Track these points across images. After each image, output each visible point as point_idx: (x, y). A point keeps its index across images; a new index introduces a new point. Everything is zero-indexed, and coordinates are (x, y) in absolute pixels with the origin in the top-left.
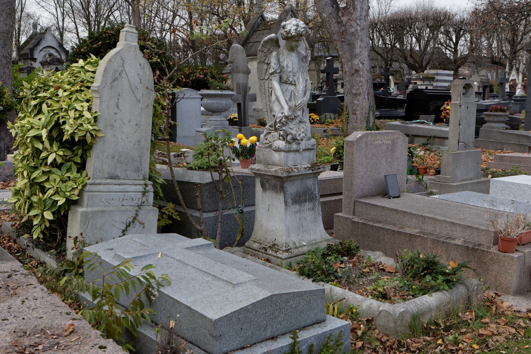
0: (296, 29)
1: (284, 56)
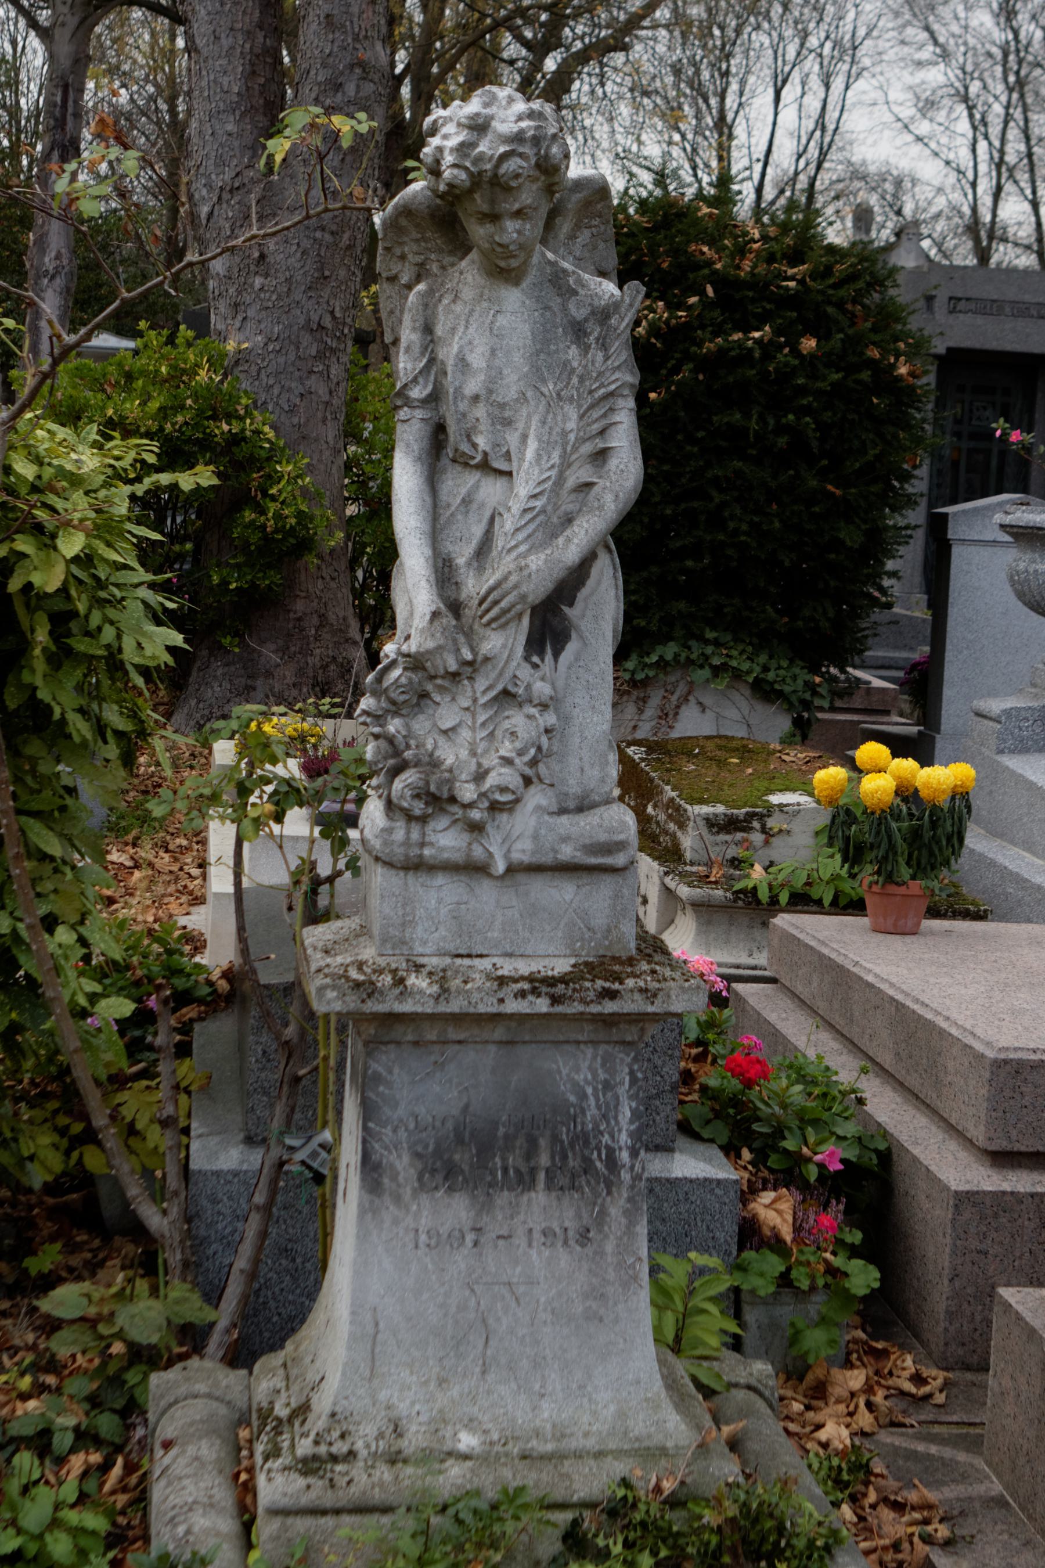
0: (463, 149)
1: (458, 308)
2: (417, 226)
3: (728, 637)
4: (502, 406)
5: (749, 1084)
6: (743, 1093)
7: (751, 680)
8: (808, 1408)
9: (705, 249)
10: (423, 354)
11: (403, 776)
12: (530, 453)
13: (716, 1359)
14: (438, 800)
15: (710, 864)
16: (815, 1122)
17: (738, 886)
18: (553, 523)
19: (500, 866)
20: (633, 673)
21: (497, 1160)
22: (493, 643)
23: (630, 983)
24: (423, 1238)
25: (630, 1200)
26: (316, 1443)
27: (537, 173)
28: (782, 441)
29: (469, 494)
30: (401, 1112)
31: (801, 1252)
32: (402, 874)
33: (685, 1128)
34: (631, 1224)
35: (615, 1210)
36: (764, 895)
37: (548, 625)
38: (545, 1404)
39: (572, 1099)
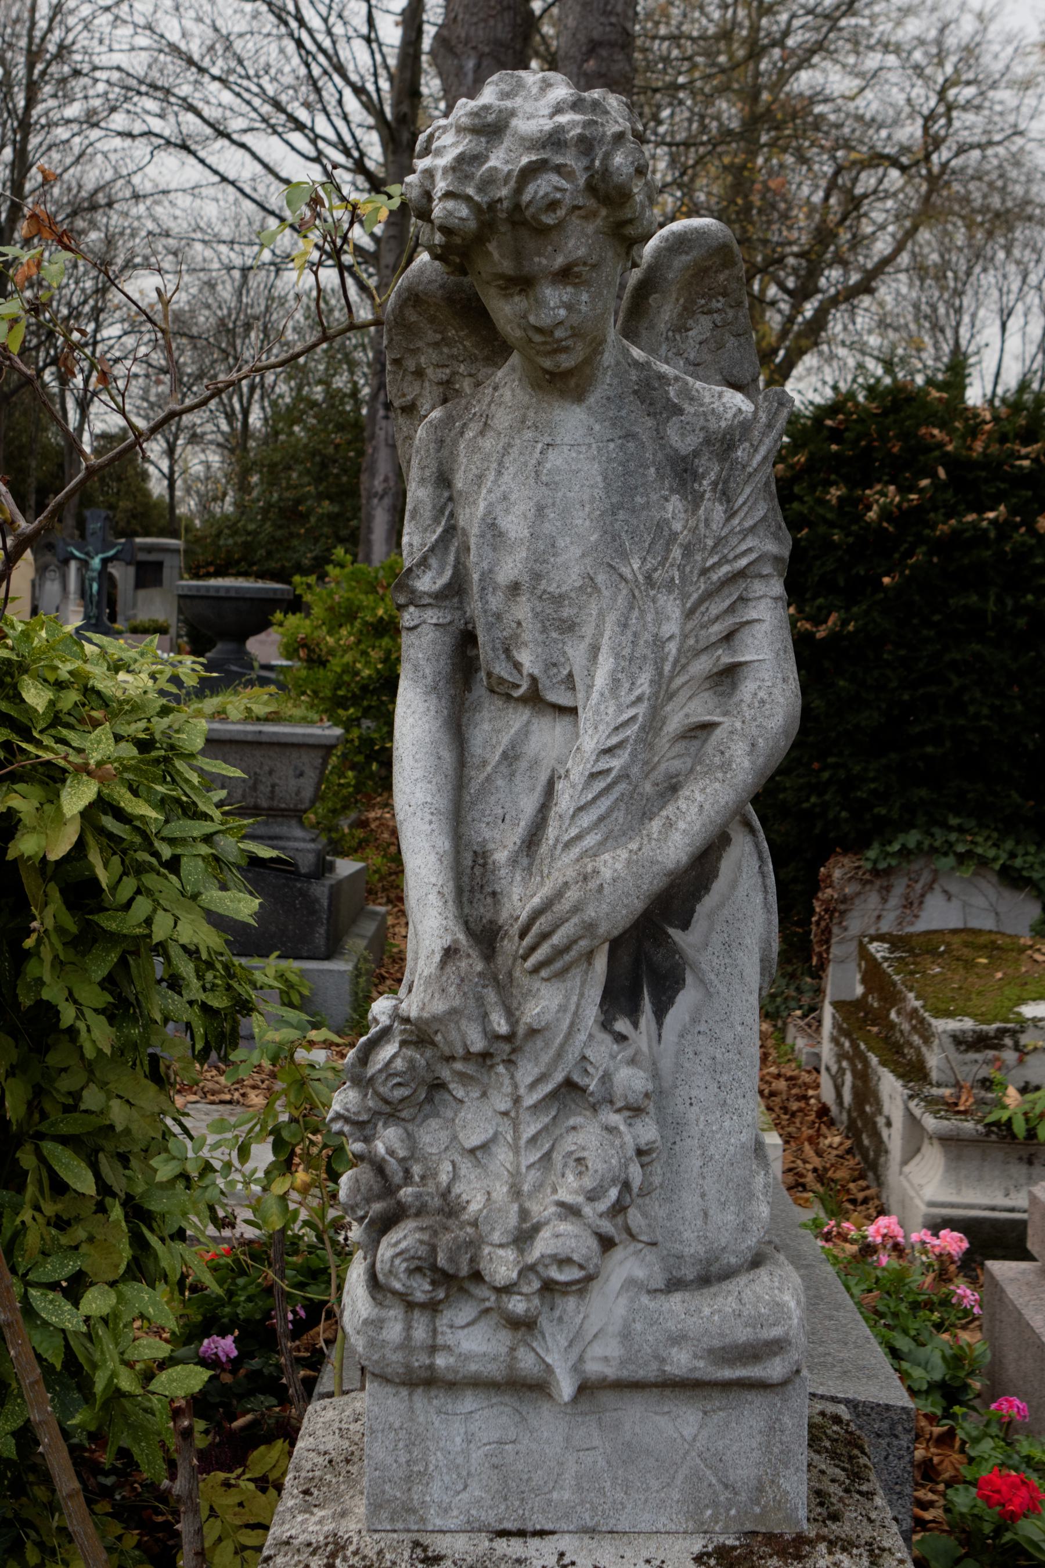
0: (463, 164)
1: (488, 443)
2: (432, 320)
3: (971, 823)
4: (558, 600)
7: (997, 866)
9: (936, 432)
10: (436, 520)
11: (393, 1236)
12: (601, 679)
14: (451, 1278)
17: (990, 1119)
18: (639, 793)
20: (875, 862)
22: (543, 1003)
27: (591, 203)
28: (1022, 622)
29: (513, 745)
32: (404, 1392)
36: (1020, 1128)
37: (643, 964)
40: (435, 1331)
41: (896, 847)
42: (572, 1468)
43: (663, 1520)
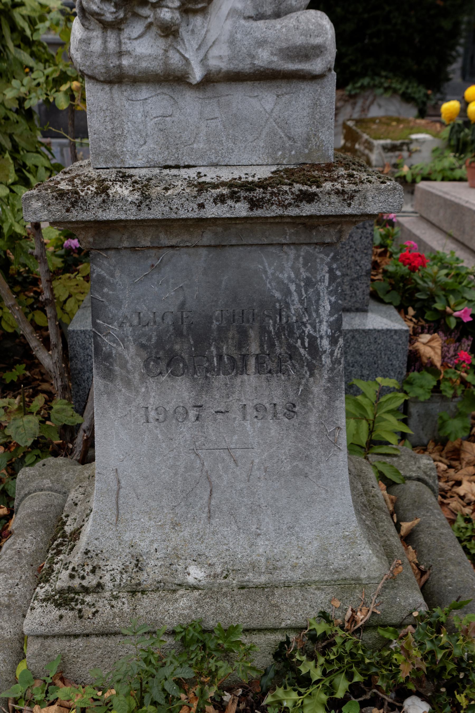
3: (391, 75)
5: (413, 269)
6: (409, 274)
8: (450, 467)
13: (395, 456)
15: (384, 166)
16: (453, 291)
19: (197, 74)
20: (350, 91)
21: (213, 349)
23: (328, 186)
24: (152, 414)
25: (330, 380)
26: (72, 577)
30: (125, 310)
31: (446, 372)
32: (107, 88)
33: (374, 296)
34: (332, 400)
35: (317, 389)
36: (409, 178)
38: (260, 542)
39: (278, 295)
40: (120, 42)
41: (359, 84)
42: (204, 130)
43: (255, 157)
